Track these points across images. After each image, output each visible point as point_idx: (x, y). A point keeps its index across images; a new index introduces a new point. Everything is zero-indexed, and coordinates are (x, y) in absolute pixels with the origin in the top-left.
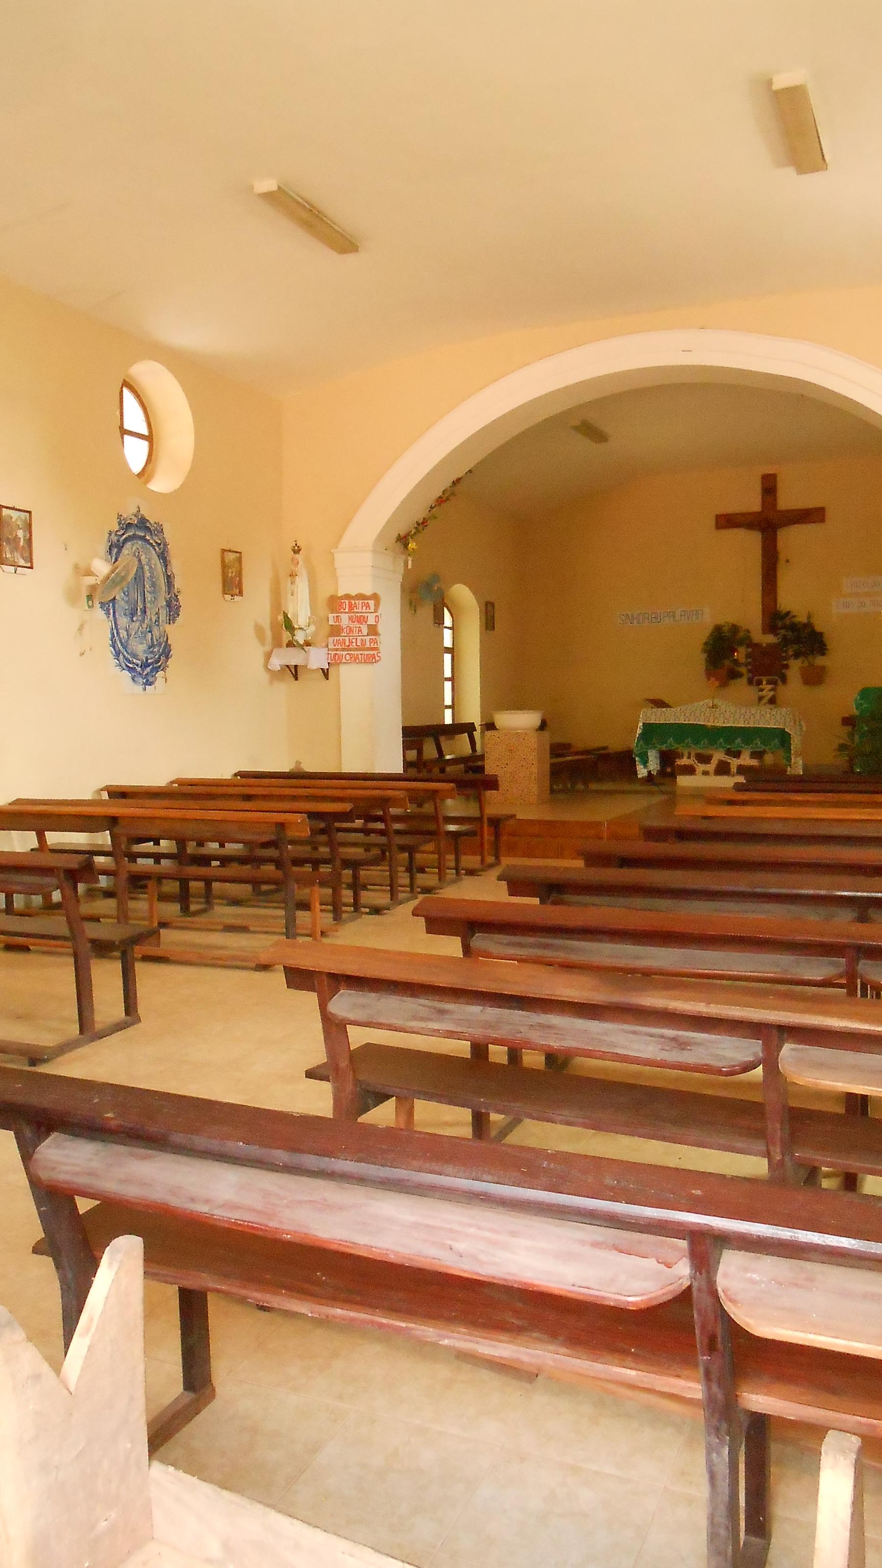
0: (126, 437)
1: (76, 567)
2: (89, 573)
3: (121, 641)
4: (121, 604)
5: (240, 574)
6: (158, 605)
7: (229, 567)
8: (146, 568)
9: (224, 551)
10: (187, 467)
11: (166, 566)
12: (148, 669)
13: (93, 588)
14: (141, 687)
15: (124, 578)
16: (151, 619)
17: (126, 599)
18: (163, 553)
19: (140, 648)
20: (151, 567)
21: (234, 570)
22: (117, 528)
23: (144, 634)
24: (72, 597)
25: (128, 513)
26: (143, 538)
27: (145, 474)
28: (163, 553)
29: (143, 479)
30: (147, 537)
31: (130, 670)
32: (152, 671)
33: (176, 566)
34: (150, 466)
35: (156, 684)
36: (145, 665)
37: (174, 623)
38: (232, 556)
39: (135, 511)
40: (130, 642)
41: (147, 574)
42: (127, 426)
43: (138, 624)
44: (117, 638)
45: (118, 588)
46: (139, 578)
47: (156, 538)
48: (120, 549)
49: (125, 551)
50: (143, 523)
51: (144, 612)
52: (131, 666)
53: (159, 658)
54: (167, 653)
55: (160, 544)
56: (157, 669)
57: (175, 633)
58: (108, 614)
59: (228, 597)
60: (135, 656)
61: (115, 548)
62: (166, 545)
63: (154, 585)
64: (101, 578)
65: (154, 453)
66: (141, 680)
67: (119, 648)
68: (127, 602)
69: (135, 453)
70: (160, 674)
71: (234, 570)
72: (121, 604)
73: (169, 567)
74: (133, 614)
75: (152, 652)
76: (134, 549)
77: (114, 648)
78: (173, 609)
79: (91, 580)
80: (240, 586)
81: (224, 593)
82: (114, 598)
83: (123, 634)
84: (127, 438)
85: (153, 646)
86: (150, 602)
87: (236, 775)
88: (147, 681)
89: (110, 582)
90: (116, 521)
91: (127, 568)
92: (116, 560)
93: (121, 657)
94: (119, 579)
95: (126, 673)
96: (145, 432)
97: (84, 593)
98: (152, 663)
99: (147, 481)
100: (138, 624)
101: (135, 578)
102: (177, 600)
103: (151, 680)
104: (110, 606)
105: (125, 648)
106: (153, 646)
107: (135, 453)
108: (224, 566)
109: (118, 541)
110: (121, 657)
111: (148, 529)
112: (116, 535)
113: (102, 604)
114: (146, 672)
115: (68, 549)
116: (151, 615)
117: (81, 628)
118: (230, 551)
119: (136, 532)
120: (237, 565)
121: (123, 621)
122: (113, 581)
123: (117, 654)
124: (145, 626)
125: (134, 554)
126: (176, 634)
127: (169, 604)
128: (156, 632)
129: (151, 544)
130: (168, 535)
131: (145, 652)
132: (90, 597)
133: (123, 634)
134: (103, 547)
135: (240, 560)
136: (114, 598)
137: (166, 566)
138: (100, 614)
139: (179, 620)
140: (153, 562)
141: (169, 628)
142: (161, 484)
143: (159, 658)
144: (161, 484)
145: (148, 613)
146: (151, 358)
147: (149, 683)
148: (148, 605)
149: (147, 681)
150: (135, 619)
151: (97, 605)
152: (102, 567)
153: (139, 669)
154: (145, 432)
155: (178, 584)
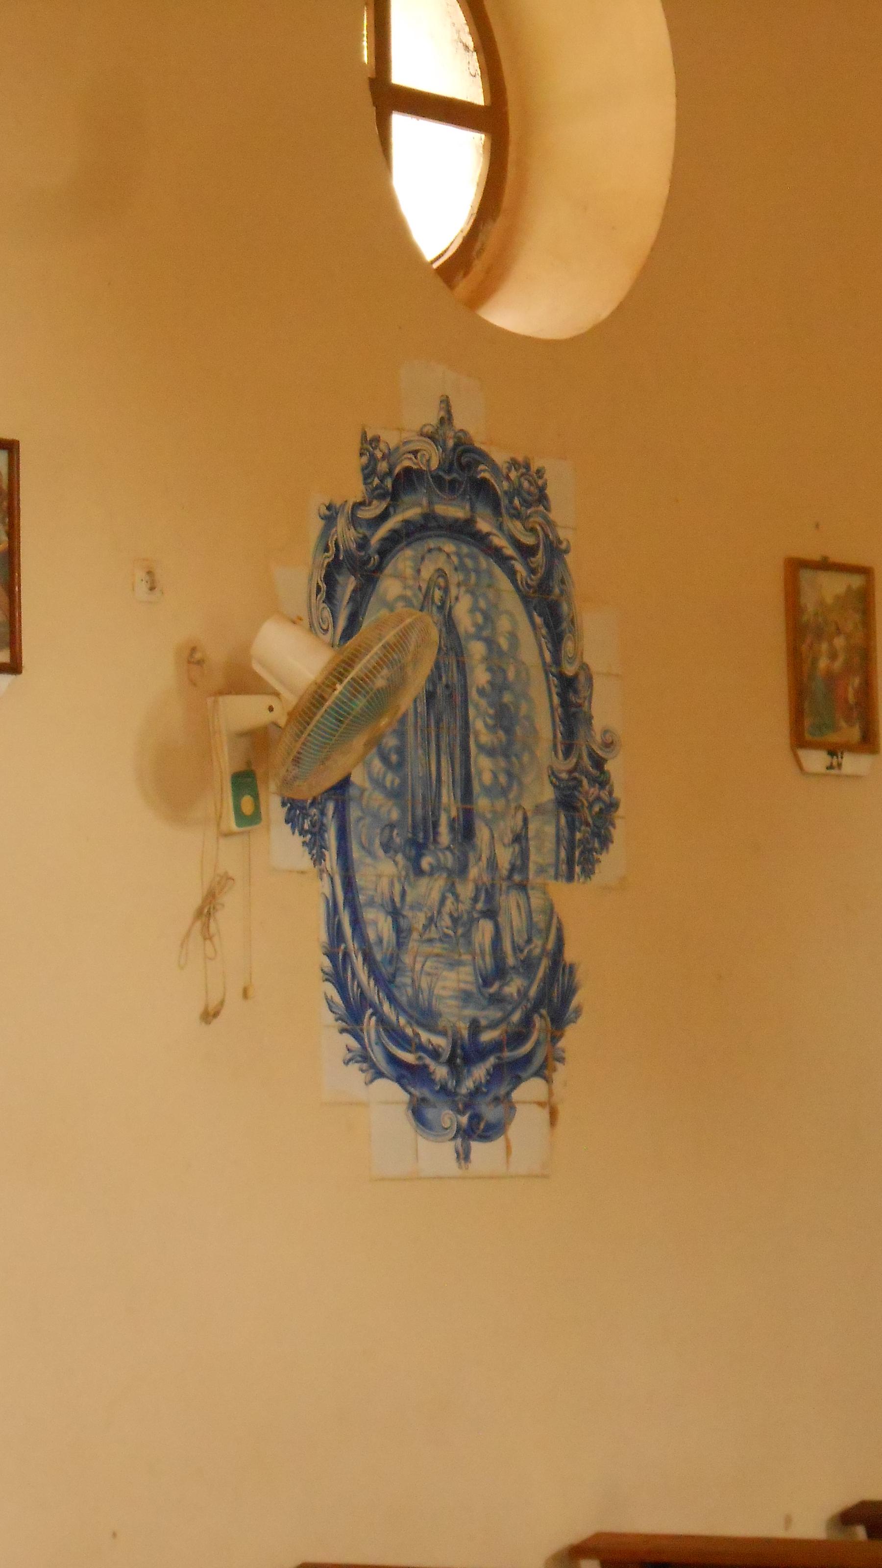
0: (404, 126)
1: (192, 659)
2: (243, 680)
3: (368, 958)
4: (373, 805)
5: (863, 658)
6: (522, 802)
7: (819, 635)
8: (477, 649)
9: (796, 567)
10: (645, 226)
11: (556, 639)
12: (480, 1072)
13: (258, 740)
14: (447, 1149)
15: (381, 701)
16: (493, 864)
17: (391, 780)
18: (544, 587)
19: (445, 983)
20: (490, 643)
21: (839, 642)
22: (356, 490)
23: (464, 925)
24: (171, 788)
25: (405, 424)
26: (462, 531)
27: (479, 258)
28: (544, 587)
29: (464, 286)
30: (484, 526)
31: (407, 1074)
32: (496, 1074)
33: (597, 641)
34: (495, 230)
35: (514, 1130)
36: (464, 1055)
37: (588, 872)
38: (832, 587)
39: (431, 417)
40: (407, 959)
41: (480, 676)
42: (402, 75)
43: (439, 883)
44: (351, 944)
45: (359, 742)
46: (445, 696)
47: (516, 527)
48: (369, 578)
49: (390, 587)
50: (462, 467)
51: (465, 830)
52: (409, 1057)
53: (527, 1021)
54: (556, 1001)
55: (527, 552)
56: (513, 1071)
57: (590, 917)
58: (315, 845)
59: (815, 760)
60: (427, 1017)
61: (349, 575)
62: (556, 551)
63: (504, 719)
64: (291, 699)
65: (511, 172)
66: (448, 1117)
67: (364, 990)
68: (396, 795)
69: (435, 182)
70: (530, 1090)
71: (839, 642)
72: (373, 805)
73: (568, 646)
74: (417, 844)
75: (496, 1000)
76: (427, 571)
77: (342, 988)
78: (585, 819)
79: (248, 711)
80: (864, 709)
81: (800, 740)
82: (344, 784)
83: (379, 925)
84: (404, 126)
85: (500, 972)
86: (488, 791)
87: (847, 1518)
88: (476, 1118)
89: (323, 715)
90: (355, 463)
91: (393, 654)
92: (348, 634)
93: (370, 1023)
94: (360, 703)
95: (389, 1091)
96: (470, 89)
97: (225, 763)
98: (496, 1047)
99: (482, 294)
100: (439, 883)
101: (431, 696)
102: (602, 781)
103: (490, 1113)
104: (322, 816)
105: (386, 983)
106: (500, 972)
107: (435, 182)
108: (800, 632)
109: (363, 544)
110: (370, 1023)
111: (482, 490)
112: (354, 521)
113: (295, 811)
114: (469, 1084)
115: (175, 580)
116: (493, 844)
117: (207, 910)
118: (825, 565)
119: (439, 505)
120: (851, 622)
121: (379, 873)
122: (340, 714)
123: (353, 1013)
124: (466, 891)
125: (427, 595)
126: (595, 920)
127: (567, 802)
128: (511, 905)
129: (496, 554)
130: (565, 512)
131: (466, 997)
132: (244, 781)
133: (379, 925)
134: (297, 578)
135: (863, 602)
136: (344, 784)
137: (556, 639)
138: (284, 846)
139: (611, 863)
140: (504, 624)
141: (572, 900)
142: (530, 308)
143: (527, 1021)
144: (530, 308)
145: (482, 834)
146: (600, 329)
147: (478, 1130)
148: (482, 803)
149: (476, 1118)
150: (426, 862)
151: (274, 809)
152: (294, 656)
153: (441, 1072)
154: (470, 89)
155: (605, 710)
